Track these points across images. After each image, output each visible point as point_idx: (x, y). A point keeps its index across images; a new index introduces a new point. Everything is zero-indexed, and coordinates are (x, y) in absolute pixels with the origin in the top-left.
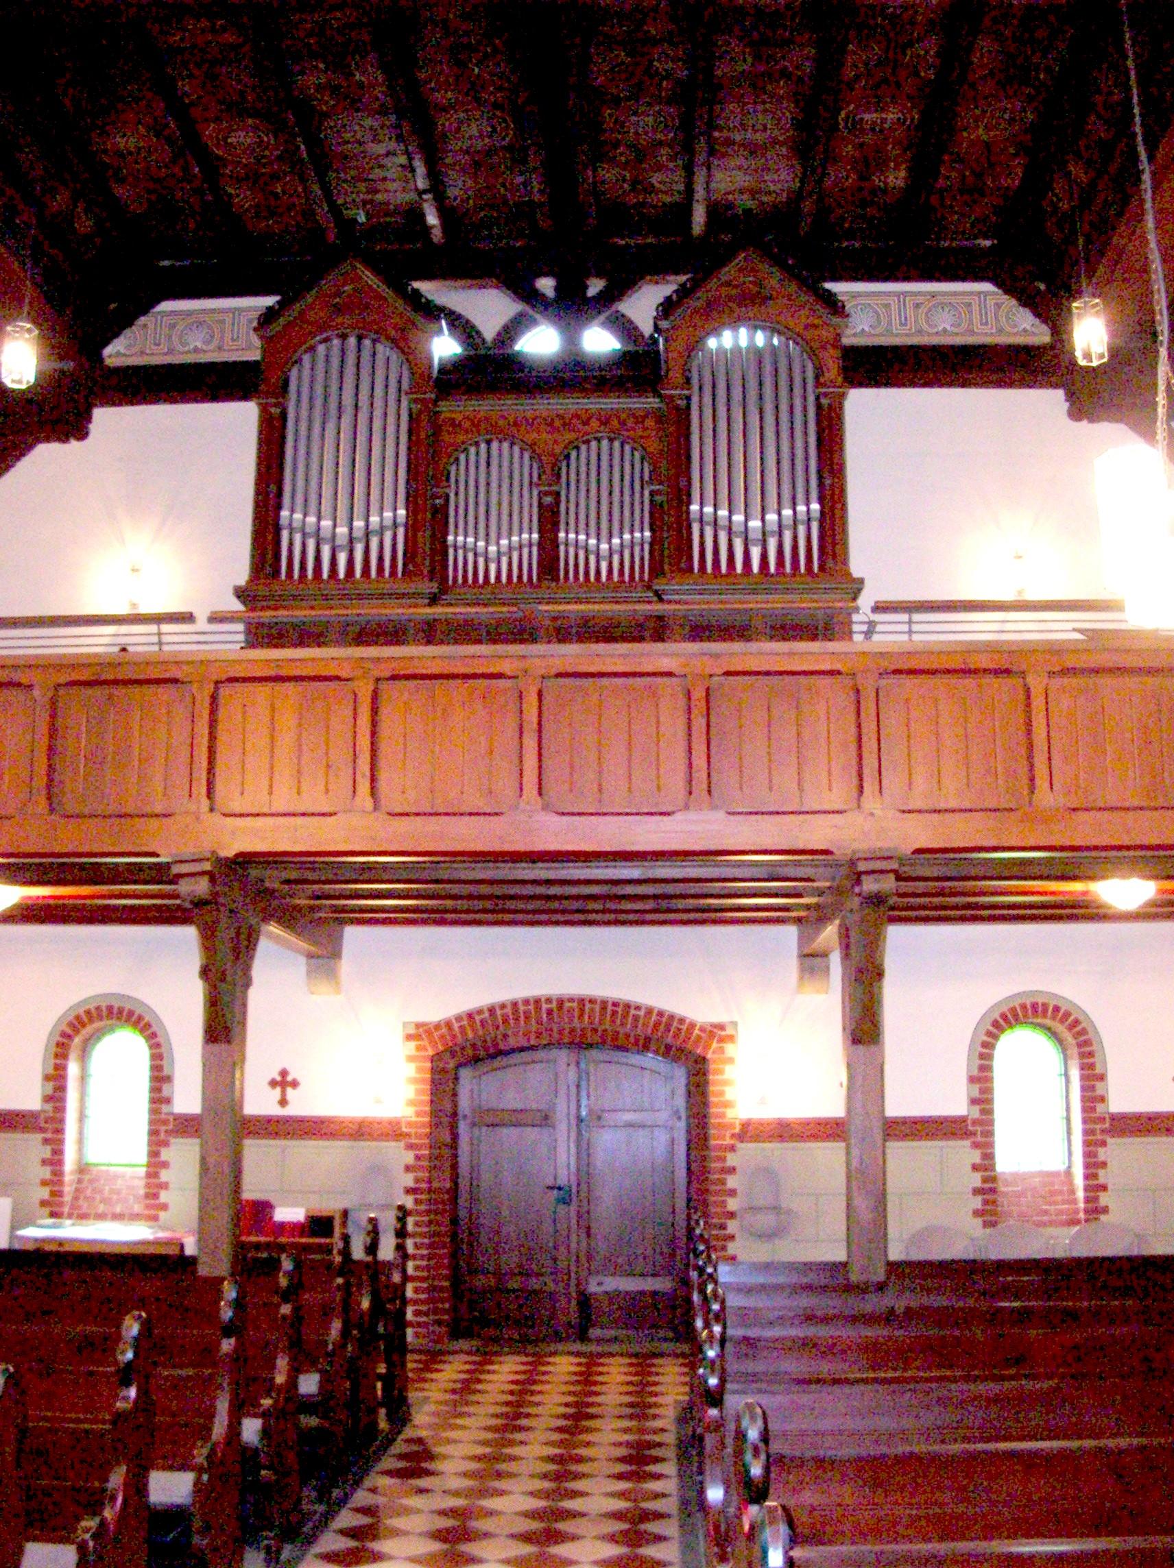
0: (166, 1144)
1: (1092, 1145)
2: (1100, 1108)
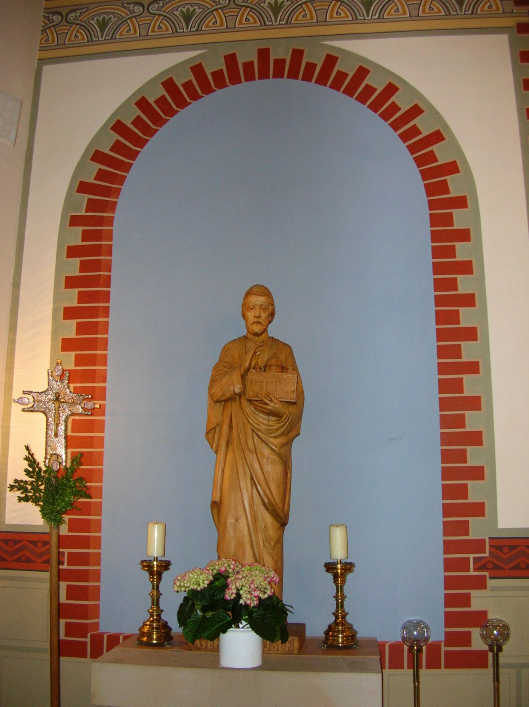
0: (480, 584)
1: (457, 588)
2: (477, 529)
